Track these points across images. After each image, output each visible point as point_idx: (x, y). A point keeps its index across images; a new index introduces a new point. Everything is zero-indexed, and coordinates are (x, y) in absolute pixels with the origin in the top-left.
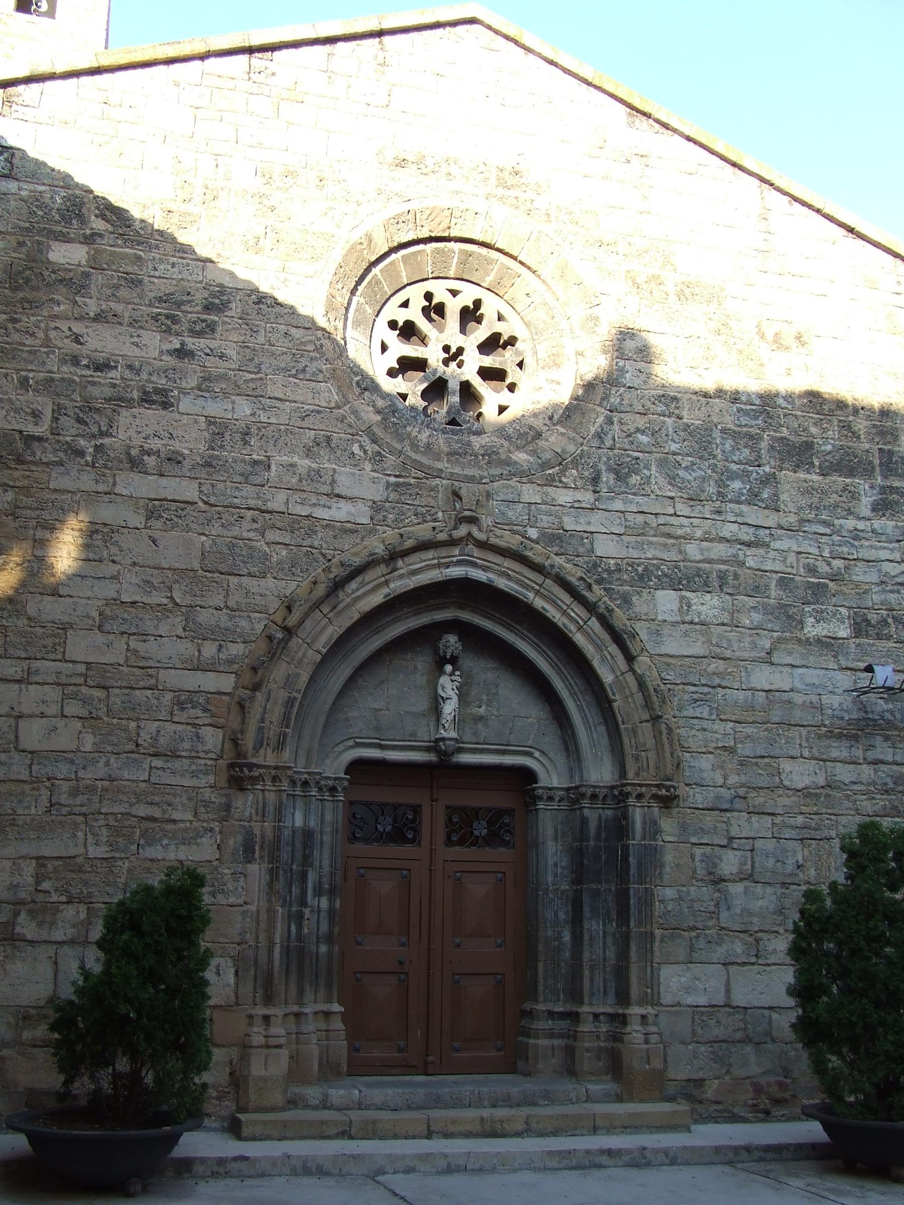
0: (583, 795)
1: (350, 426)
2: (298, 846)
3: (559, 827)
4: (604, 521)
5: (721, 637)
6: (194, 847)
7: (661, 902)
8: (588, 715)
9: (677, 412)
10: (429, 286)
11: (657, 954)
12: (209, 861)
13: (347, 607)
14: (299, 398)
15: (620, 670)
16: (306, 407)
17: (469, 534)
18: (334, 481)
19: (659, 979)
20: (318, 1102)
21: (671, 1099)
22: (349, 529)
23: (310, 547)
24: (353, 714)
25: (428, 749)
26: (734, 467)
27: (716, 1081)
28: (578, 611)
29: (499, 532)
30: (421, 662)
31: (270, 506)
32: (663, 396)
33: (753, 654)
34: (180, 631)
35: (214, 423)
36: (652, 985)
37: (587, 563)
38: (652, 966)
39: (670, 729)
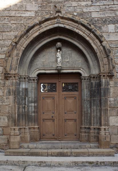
0: (91, 77)
3: (87, 86)
8: (92, 58)
11: (108, 113)
13: (30, 36)
18: (26, 7)
19: (109, 120)
21: (112, 148)
22: (30, 18)
25: (56, 70)
28: (87, 32)
30: (53, 50)
31: (11, 15)
36: (107, 121)
37: (89, 20)
38: (107, 117)
39: (112, 59)
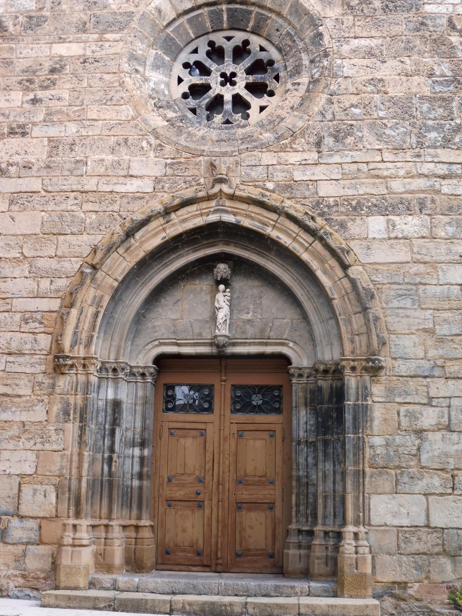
1: (141, 130)
2: (109, 411)
4: (325, 172)
5: (420, 247)
6: (32, 412)
7: (371, 447)
9: (383, 89)
10: (212, 37)
12: (41, 422)
14: (107, 117)
15: (338, 277)
16: (112, 122)
17: (221, 191)
20: (109, 585)
22: (138, 197)
23: (112, 211)
24: (157, 323)
25: (211, 344)
26: (430, 123)
27: (417, 584)
29: (242, 187)
30: (203, 285)
31: (86, 188)
32: (372, 79)
33: (448, 258)
34: (27, 274)
35: (52, 141)
36: (364, 510)
38: (363, 496)
